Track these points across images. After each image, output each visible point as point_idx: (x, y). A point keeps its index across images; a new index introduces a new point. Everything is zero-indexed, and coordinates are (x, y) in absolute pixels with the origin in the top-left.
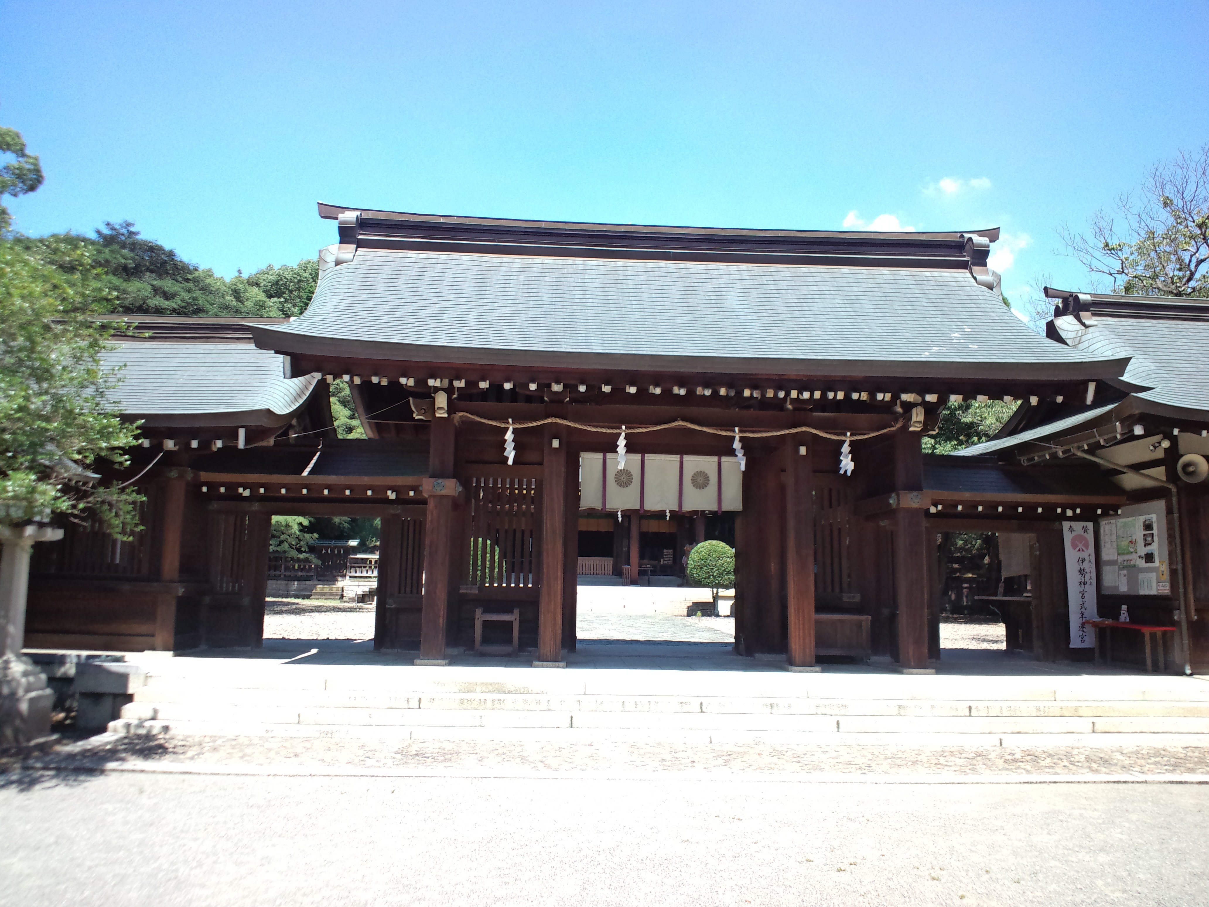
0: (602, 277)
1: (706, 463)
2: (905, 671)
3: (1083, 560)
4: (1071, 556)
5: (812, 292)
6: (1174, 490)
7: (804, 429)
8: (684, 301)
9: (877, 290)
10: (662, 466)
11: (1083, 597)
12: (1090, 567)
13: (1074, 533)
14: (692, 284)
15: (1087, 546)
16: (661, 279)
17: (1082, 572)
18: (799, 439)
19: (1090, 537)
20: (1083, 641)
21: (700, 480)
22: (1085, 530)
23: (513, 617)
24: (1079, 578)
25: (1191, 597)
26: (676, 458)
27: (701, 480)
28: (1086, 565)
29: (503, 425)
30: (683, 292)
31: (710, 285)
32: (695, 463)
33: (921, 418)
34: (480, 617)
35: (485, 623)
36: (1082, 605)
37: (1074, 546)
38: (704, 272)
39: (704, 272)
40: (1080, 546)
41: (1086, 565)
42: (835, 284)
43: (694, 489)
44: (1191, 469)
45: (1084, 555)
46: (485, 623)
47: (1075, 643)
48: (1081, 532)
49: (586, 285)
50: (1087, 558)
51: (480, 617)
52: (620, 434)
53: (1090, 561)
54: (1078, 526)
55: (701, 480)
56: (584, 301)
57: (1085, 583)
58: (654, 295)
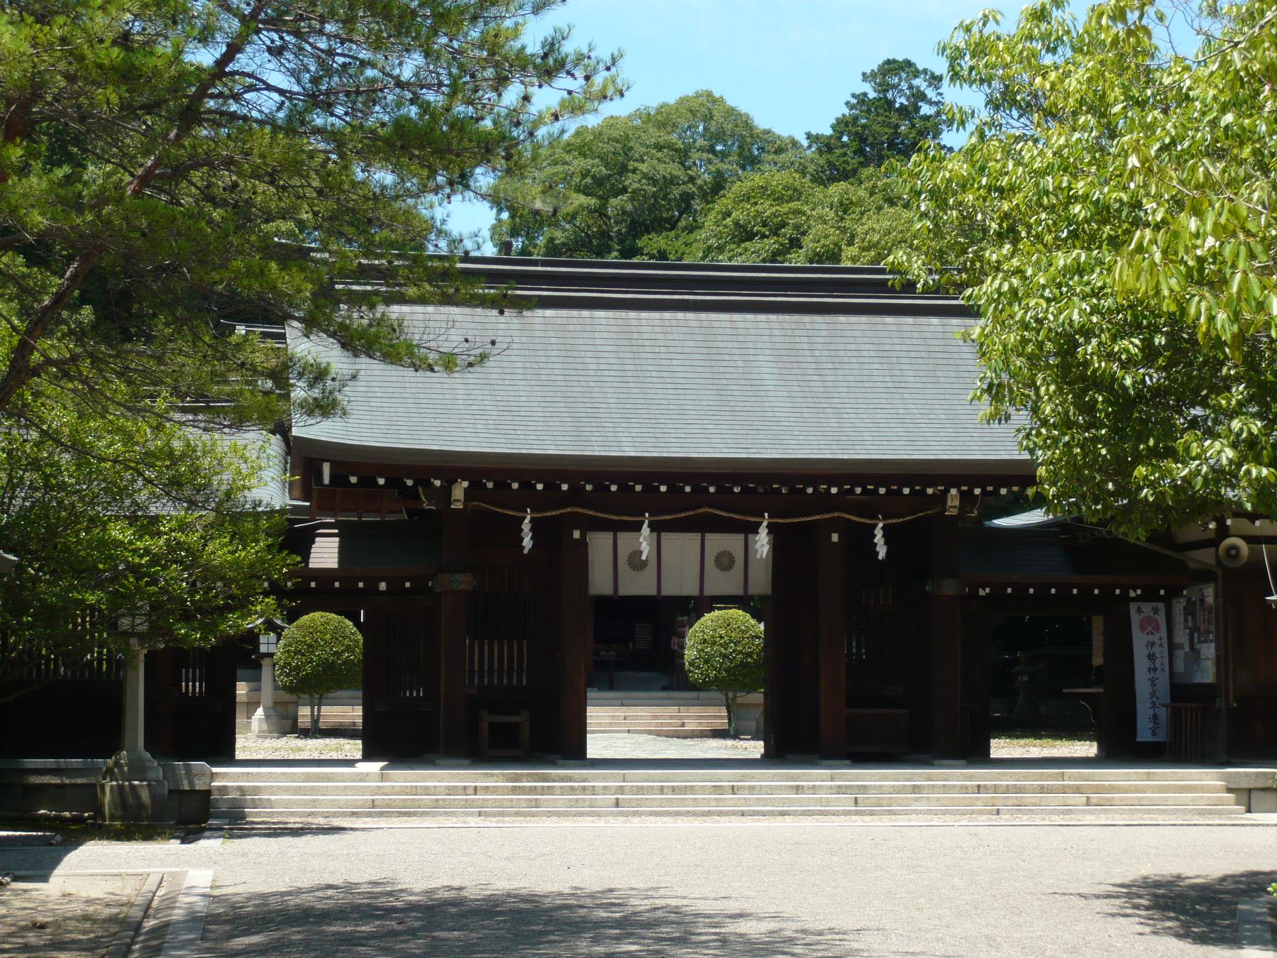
0: (614, 335)
1: (732, 542)
2: (936, 762)
3: (1153, 644)
4: (1139, 641)
5: (849, 353)
6: (1220, 573)
7: (836, 514)
8: (707, 369)
9: (921, 348)
10: (682, 546)
11: (1153, 685)
12: (1162, 652)
13: (1143, 615)
14: (716, 344)
15: (1157, 628)
16: (681, 337)
17: (1151, 657)
18: (833, 525)
19: (1161, 618)
20: (1154, 734)
21: (725, 561)
22: (1156, 611)
23: (522, 718)
24: (1147, 664)
25: (1231, 685)
26: (696, 537)
27: (725, 561)
28: (1156, 649)
29: (520, 515)
30: (706, 357)
31: (735, 345)
32: (718, 542)
33: (957, 503)
34: (486, 718)
35: (491, 724)
36: (1153, 694)
37: (1142, 628)
38: (728, 325)
39: (728, 325)
40: (1149, 629)
41: (1156, 649)
42: (876, 341)
43: (718, 571)
44: (1233, 552)
45: (1155, 638)
46: (491, 724)
47: (1144, 733)
48: (1151, 614)
49: (598, 348)
50: (1158, 642)
51: (486, 718)
52: (643, 522)
53: (1161, 645)
54: (1147, 607)
55: (725, 561)
56: (599, 373)
57: (1155, 670)
58: (675, 362)
